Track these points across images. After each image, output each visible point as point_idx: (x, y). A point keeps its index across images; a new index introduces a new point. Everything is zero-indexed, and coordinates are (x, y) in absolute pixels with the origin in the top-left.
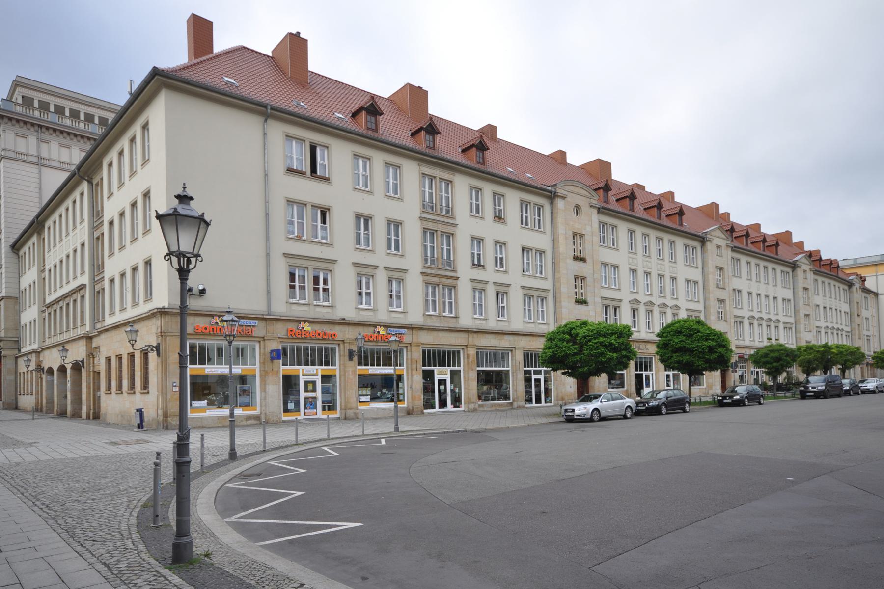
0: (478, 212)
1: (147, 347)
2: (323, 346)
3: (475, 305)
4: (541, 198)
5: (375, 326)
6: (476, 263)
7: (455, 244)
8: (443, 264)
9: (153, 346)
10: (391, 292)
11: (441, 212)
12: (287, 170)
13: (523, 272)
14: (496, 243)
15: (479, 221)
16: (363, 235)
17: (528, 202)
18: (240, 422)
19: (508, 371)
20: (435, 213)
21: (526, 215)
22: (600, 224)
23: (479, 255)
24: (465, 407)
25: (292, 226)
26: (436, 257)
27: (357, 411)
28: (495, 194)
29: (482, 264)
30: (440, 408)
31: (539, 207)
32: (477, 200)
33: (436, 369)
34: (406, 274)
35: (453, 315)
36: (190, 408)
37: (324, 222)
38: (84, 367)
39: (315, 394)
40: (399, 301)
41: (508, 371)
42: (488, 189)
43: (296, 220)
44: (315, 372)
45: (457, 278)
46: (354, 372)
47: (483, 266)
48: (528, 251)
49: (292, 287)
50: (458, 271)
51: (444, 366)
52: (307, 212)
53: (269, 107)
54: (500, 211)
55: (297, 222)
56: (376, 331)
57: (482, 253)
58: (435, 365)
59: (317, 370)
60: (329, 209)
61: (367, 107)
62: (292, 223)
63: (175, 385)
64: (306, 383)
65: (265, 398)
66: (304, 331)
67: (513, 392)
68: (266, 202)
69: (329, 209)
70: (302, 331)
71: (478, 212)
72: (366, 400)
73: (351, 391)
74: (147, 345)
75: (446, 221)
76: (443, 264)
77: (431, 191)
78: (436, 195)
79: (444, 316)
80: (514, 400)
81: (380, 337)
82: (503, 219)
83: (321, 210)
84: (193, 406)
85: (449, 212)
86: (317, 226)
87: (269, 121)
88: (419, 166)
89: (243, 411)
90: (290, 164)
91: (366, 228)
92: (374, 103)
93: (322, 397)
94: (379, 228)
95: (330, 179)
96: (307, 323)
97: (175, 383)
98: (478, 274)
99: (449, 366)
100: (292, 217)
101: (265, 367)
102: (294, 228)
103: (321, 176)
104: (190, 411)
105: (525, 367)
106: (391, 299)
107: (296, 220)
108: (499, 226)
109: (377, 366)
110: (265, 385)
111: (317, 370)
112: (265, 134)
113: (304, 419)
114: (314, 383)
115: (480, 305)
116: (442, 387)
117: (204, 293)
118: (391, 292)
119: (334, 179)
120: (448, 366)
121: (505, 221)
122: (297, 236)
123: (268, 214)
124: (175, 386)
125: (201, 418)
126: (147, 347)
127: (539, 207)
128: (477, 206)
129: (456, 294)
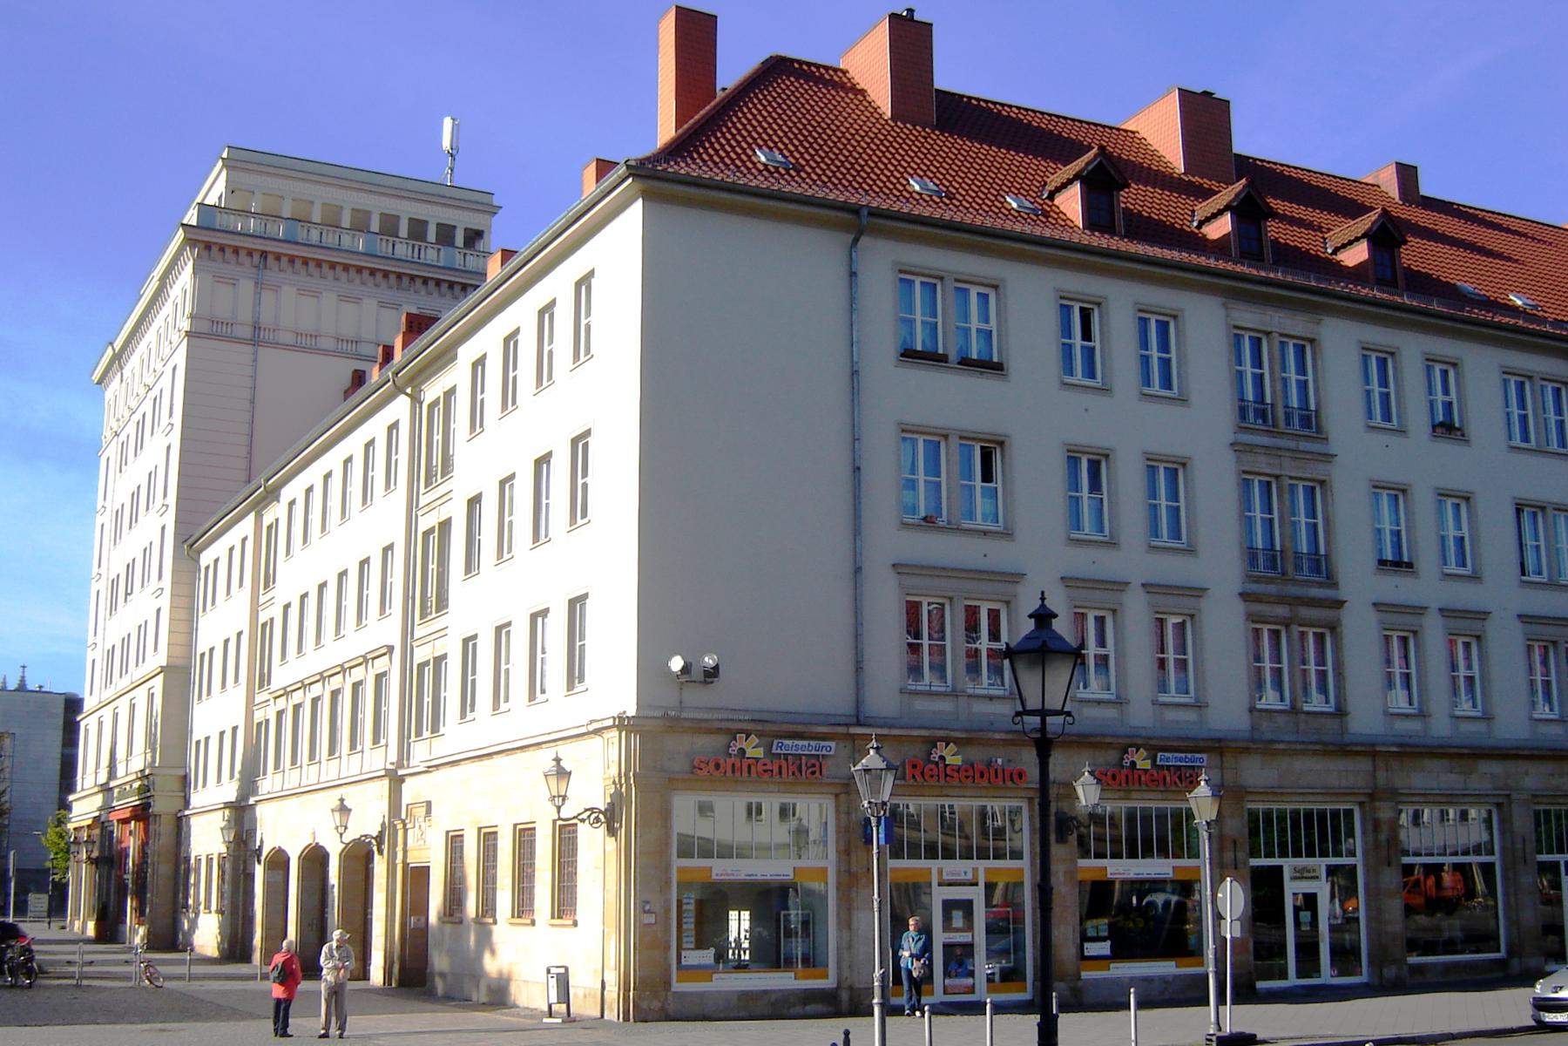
0: (1387, 416)
1: (588, 813)
2: (1275, 807)
3: (1532, 683)
4: (1068, 273)
5: (733, 734)
6: (1390, 558)
7: (1330, 508)
8: (1298, 568)
9: (601, 812)
10: (1163, 652)
11: (1288, 424)
12: (902, 355)
13: (1523, 574)
14: (1443, 494)
15: (1176, 410)
16: (1086, 502)
17: (1387, 352)
18: (789, 1008)
19: (1354, 867)
20: (1271, 429)
21: (1385, 390)
22: (1505, 382)
23: (1460, 541)
24: (1371, 975)
25: (912, 492)
26: (1278, 548)
27: (1080, 984)
28: (1430, 360)
29: (1406, 560)
30: (1299, 976)
31: (1557, 385)
32: (1384, 382)
33: (1288, 864)
34: (1201, 599)
35: (1330, 708)
36: (677, 969)
37: (987, 476)
38: (259, 862)
39: (970, 934)
40: (1182, 675)
41: (1354, 867)
42: (1413, 347)
43: (921, 477)
44: (970, 876)
45: (1339, 604)
46: (1071, 874)
47: (1410, 565)
48: (1535, 514)
49: (915, 649)
50: (1341, 583)
51: (1311, 854)
52: (949, 455)
53: (865, 212)
54: (1448, 406)
55: (925, 481)
56: (734, 750)
57: (1403, 528)
58: (1283, 854)
59: (975, 870)
60: (1001, 444)
61: (1089, 173)
62: (912, 485)
63: (647, 908)
64: (949, 906)
65: (850, 947)
66: (946, 766)
67: (1507, 928)
68: (855, 440)
69: (1001, 444)
70: (941, 765)
71: (1387, 416)
72: (702, 962)
73: (1062, 928)
74: (587, 807)
75: (1301, 448)
76: (1298, 568)
77: (1385, 390)
78: (1272, 380)
79: (1308, 713)
80: (1511, 952)
81: (1136, 777)
82: (1458, 429)
83: (982, 447)
84: (684, 963)
85: (1310, 421)
86: (971, 488)
87: (865, 241)
88: (1226, 308)
89: (1177, 966)
90: (908, 337)
91: (1095, 485)
92: (1253, 194)
93: (1330, 938)
94: (1127, 479)
95: (1005, 366)
96: (1142, 750)
97: (648, 902)
98: (1396, 588)
99: (1324, 854)
100: (913, 470)
101: (849, 863)
102: (917, 497)
103: (982, 361)
104: (678, 977)
105: (1254, 853)
106: (1162, 671)
107: (921, 477)
108: (1448, 449)
109: (1265, 857)
110: (849, 909)
111: (975, 870)
112: (853, 274)
113: (942, 1003)
114: (966, 907)
115: (1182, 665)
116: (1305, 916)
117: (715, 677)
118: (1163, 652)
119: (1014, 363)
120: (1321, 856)
121: (1463, 435)
122: (925, 519)
123: (859, 468)
124: (649, 912)
125: (701, 995)
126: (588, 813)
127: (1557, 385)
128: (1385, 398)
129: (1337, 649)
